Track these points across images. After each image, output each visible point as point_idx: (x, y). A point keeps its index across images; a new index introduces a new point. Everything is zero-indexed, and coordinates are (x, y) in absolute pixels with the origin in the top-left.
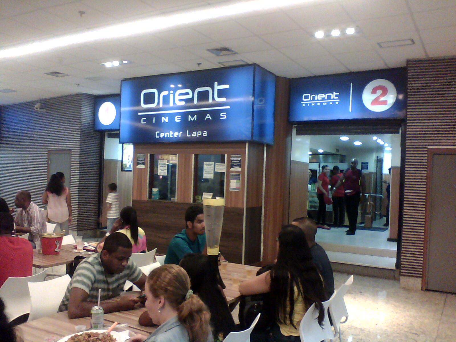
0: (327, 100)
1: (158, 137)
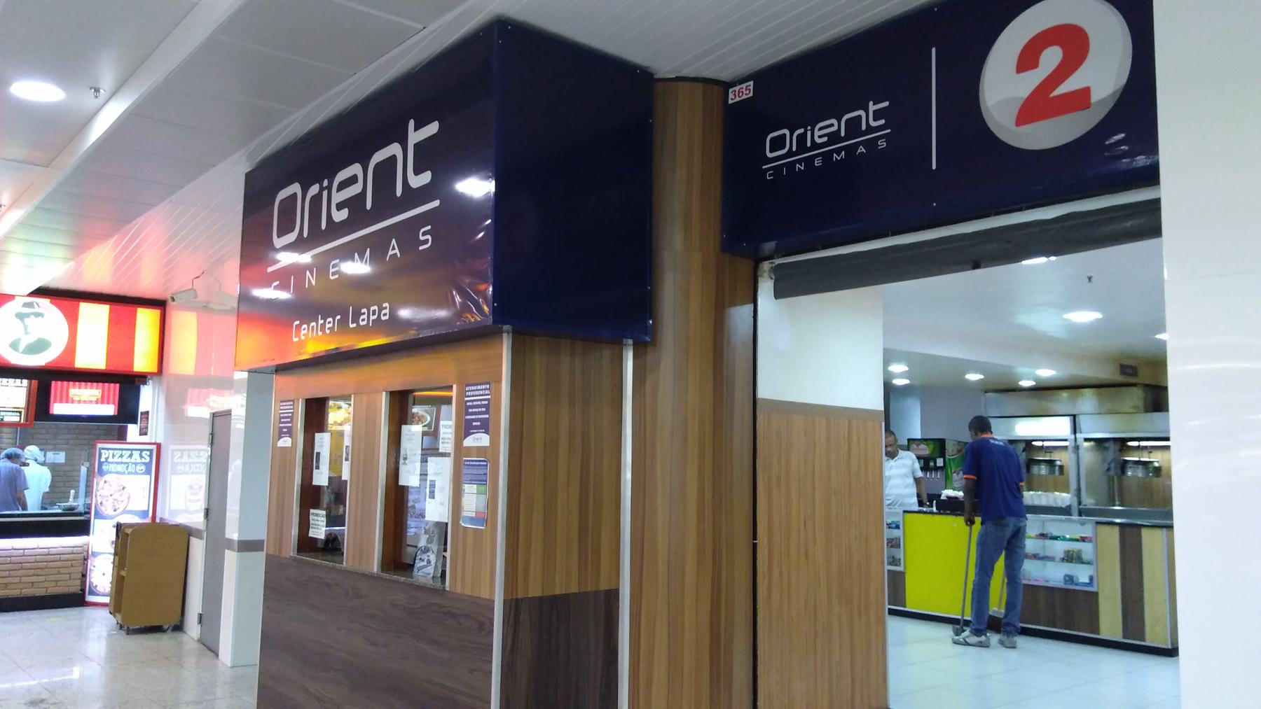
0: (847, 138)
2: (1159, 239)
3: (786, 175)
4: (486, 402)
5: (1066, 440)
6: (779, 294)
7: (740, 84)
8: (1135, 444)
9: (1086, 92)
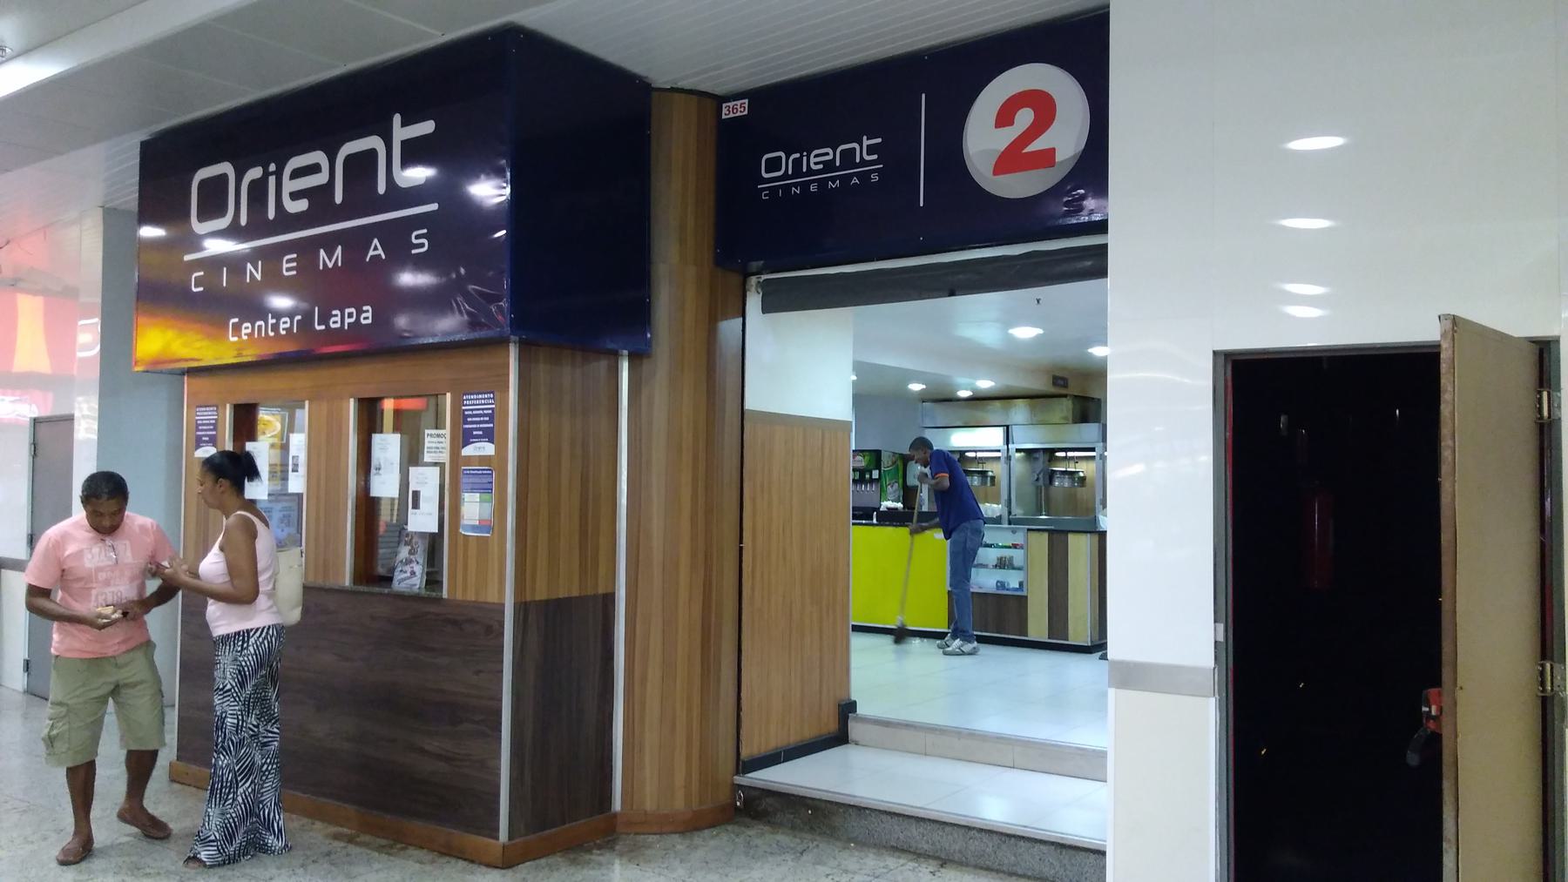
1: (323, 327)
2: (1105, 279)
3: (781, 197)
4: (490, 412)
5: (999, 451)
6: (767, 308)
7: (734, 101)
8: (1062, 454)
9: (1051, 152)
